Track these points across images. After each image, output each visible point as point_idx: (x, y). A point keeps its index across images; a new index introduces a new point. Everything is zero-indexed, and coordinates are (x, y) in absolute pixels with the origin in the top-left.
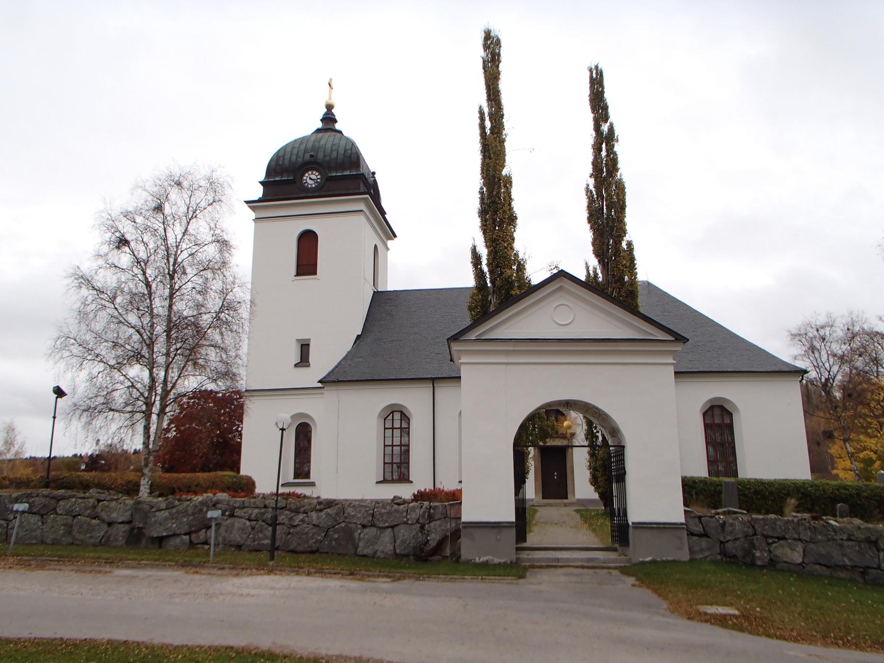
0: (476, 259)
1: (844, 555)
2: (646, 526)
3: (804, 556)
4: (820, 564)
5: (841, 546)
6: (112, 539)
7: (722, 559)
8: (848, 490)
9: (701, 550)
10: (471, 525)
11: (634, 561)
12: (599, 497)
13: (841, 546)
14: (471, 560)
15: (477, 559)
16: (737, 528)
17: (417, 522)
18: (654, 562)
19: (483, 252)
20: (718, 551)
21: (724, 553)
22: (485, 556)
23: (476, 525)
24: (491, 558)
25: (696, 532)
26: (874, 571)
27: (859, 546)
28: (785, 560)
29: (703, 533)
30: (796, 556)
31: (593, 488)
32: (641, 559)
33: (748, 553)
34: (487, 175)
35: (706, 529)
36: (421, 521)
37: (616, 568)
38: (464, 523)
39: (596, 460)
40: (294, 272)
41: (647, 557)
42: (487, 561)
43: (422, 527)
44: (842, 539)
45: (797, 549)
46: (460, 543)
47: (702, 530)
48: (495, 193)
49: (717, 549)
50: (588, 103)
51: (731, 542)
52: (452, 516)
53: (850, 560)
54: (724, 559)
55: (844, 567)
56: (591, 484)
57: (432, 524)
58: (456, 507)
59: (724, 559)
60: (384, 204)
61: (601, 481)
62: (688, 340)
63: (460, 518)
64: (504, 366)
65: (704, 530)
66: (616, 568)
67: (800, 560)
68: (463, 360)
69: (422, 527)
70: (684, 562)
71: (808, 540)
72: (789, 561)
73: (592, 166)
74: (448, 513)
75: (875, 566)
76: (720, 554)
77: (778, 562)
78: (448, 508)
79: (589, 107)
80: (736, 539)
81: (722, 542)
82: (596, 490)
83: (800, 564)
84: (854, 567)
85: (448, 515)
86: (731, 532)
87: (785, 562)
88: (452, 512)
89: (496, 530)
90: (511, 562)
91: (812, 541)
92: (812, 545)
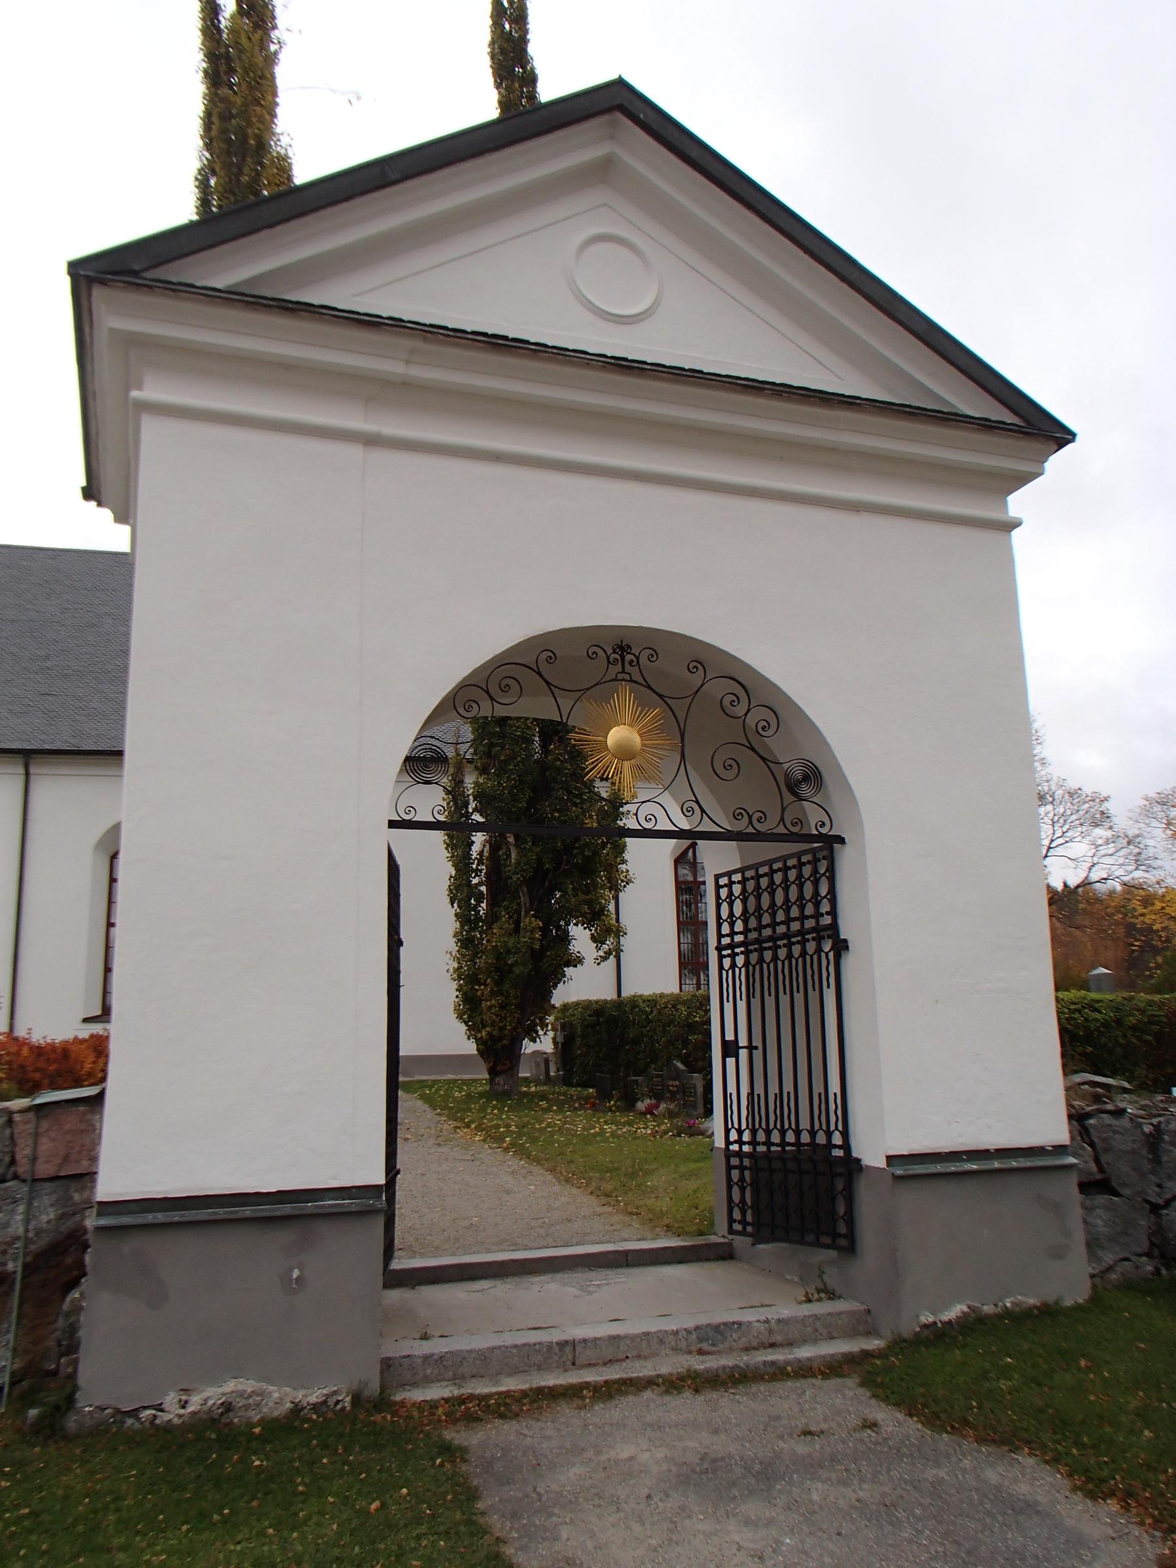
2: (939, 1168)
6: (1115, 918)
7: (1157, 1272)
8: (1100, 1012)
10: (150, 1218)
11: (908, 1328)
12: (478, 1050)
14: (134, 1413)
15: (170, 1400)
18: (972, 1324)
20: (1145, 1245)
22: (215, 1381)
23: (176, 1216)
24: (249, 1385)
29: (1099, 1177)
31: (464, 1027)
32: (927, 1318)
34: (224, 131)
35: (1104, 1159)
37: (833, 1368)
38: (106, 1208)
39: (475, 955)
41: (947, 1307)
42: (228, 1407)
46: (77, 1309)
47: (1093, 1167)
48: (245, 179)
50: (487, 61)
52: (45, 1169)
54: (1164, 1272)
56: (460, 1017)
58: (70, 1121)
59: (1164, 1272)
61: (490, 1008)
62: (1060, 435)
63: (88, 1177)
64: (355, 452)
65: (1101, 1169)
66: (833, 1368)
68: (153, 390)
70: (1078, 1308)
74: (23, 1152)
76: (1148, 1255)
78: (24, 1126)
79: (489, 73)
81: (1155, 1208)
82: (473, 1029)
85: (22, 1168)
88: (45, 1145)
89: (285, 1236)
90: (357, 1399)
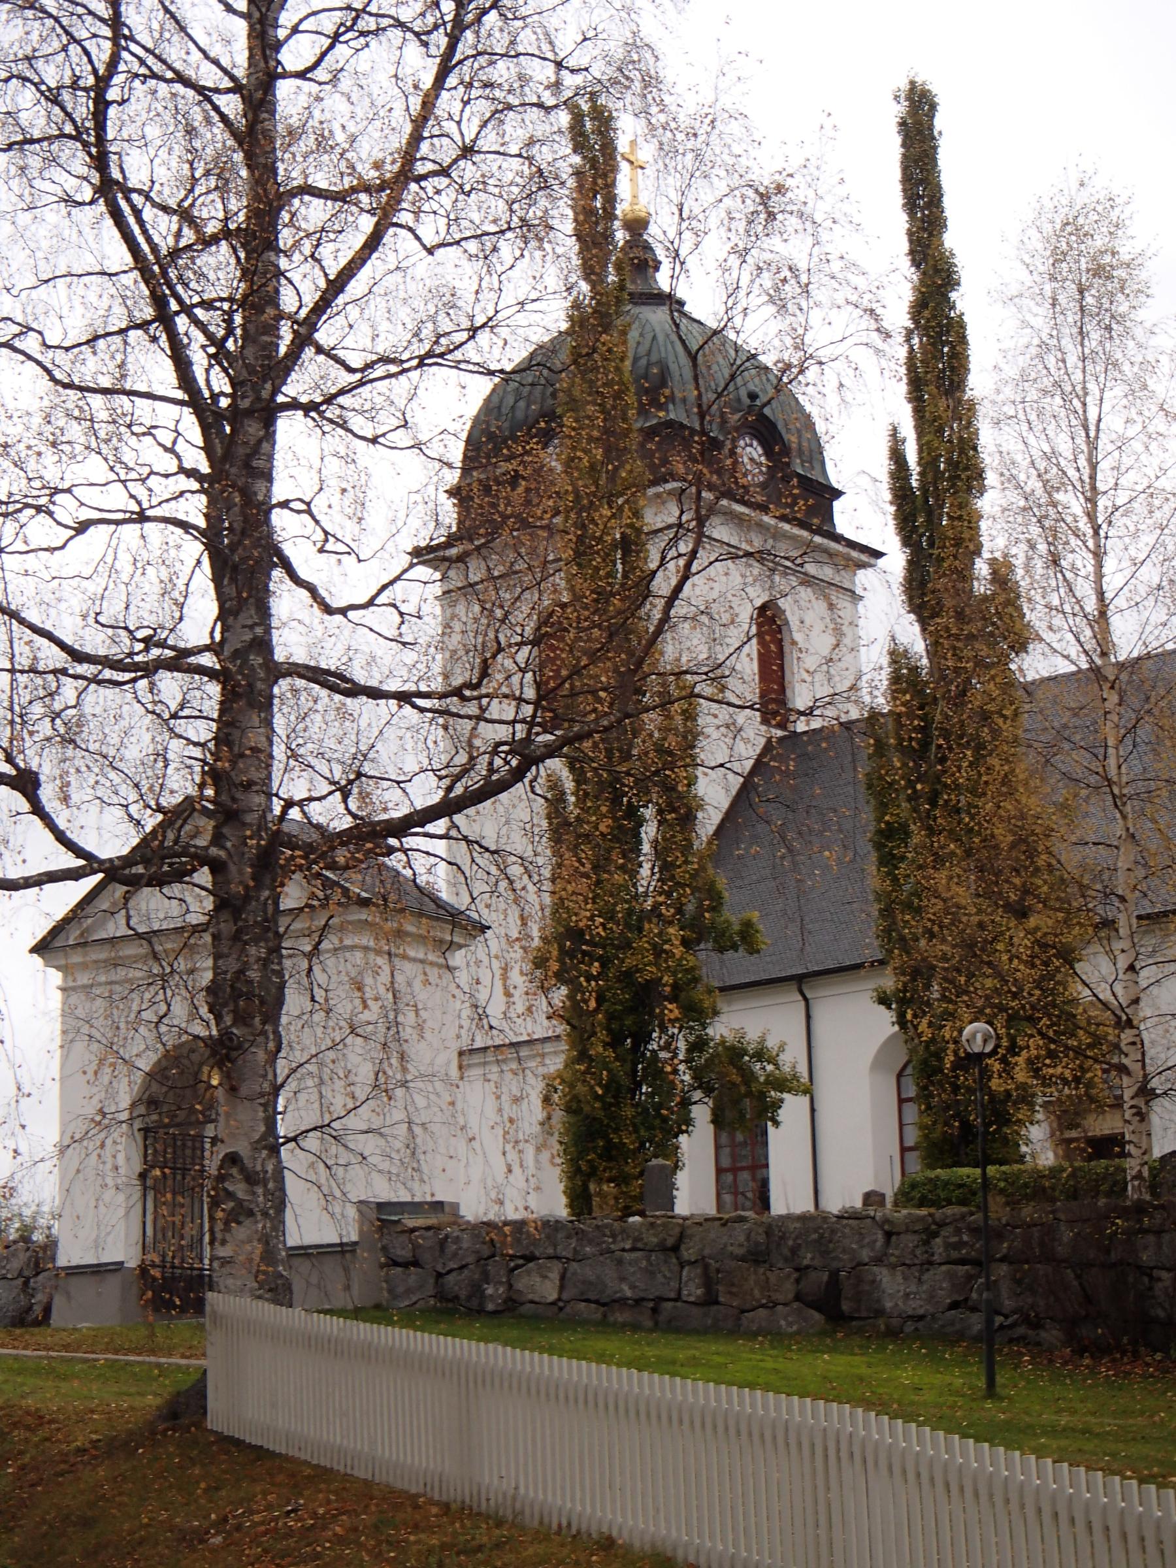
0: (897, 456)
1: (623, 1279)
3: (562, 1288)
4: (587, 1301)
5: (620, 1262)
9: (409, 1291)
13: (620, 1262)
16: (465, 1245)
17: (20, 1275)
19: (908, 431)
21: (441, 1296)
25: (400, 1260)
26: (670, 1305)
27: (648, 1260)
28: (530, 1297)
30: (549, 1290)
33: (477, 1290)
36: (26, 1273)
40: (842, 498)
43: (26, 1283)
44: (623, 1250)
45: (550, 1275)
49: (430, 1289)
51: (454, 1274)
53: (633, 1287)
55: (622, 1302)
57: (40, 1277)
60: (695, 316)
67: (553, 1296)
69: (26, 1283)
71: (570, 1256)
72: (537, 1299)
73: (898, 140)
75: (673, 1295)
77: (522, 1304)
80: (462, 1267)
81: (439, 1275)
83: (553, 1303)
84: (638, 1301)
86: (455, 1255)
87: (532, 1302)
91: (577, 1258)
92: (574, 1265)
